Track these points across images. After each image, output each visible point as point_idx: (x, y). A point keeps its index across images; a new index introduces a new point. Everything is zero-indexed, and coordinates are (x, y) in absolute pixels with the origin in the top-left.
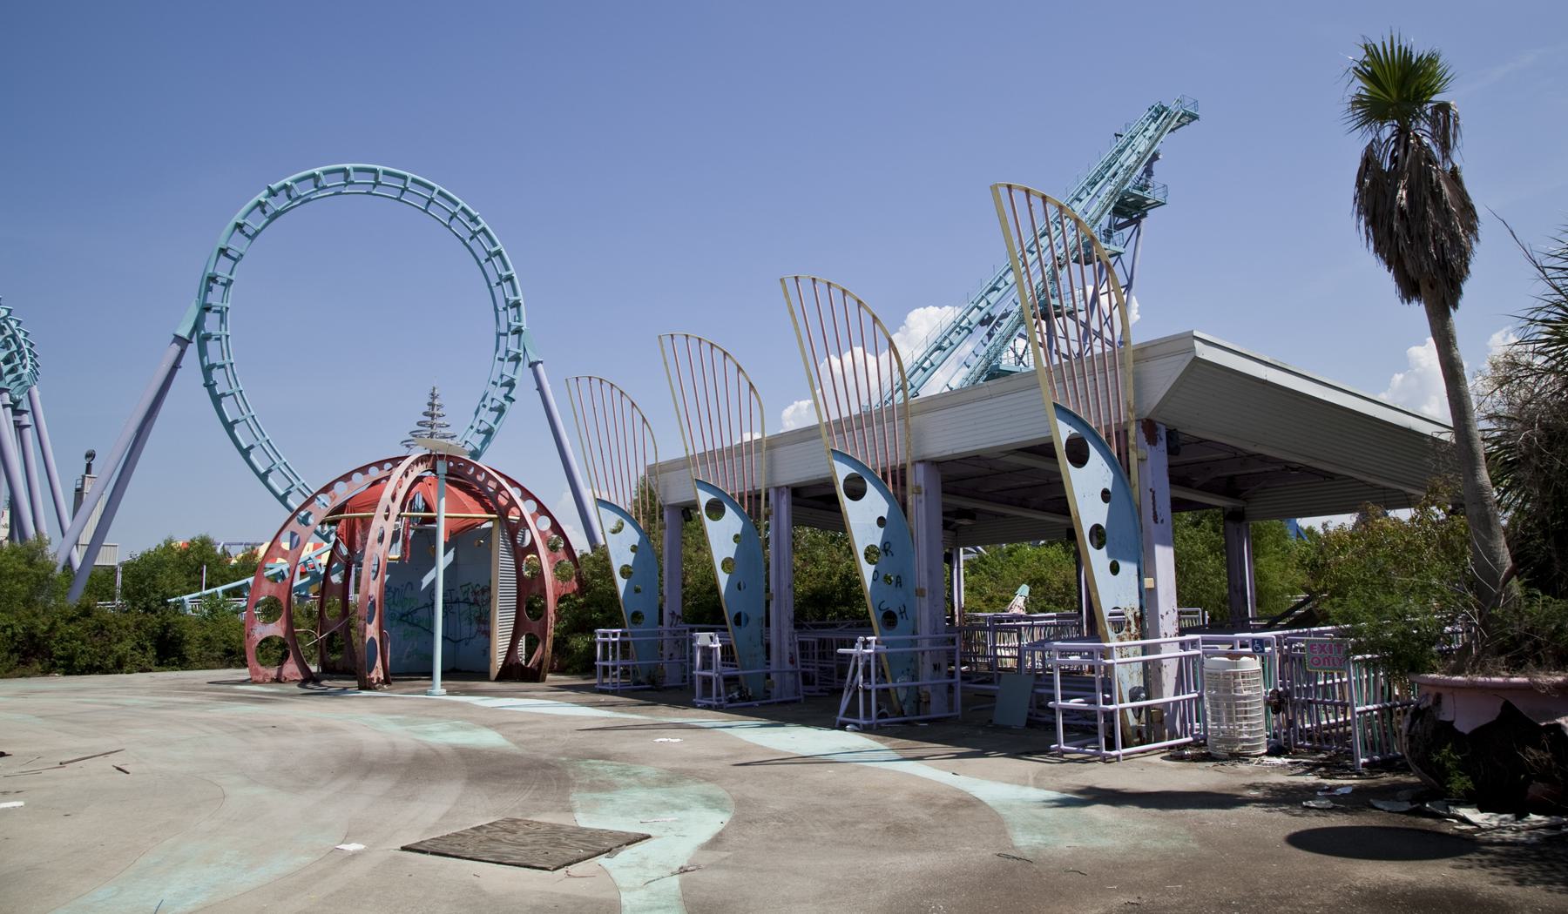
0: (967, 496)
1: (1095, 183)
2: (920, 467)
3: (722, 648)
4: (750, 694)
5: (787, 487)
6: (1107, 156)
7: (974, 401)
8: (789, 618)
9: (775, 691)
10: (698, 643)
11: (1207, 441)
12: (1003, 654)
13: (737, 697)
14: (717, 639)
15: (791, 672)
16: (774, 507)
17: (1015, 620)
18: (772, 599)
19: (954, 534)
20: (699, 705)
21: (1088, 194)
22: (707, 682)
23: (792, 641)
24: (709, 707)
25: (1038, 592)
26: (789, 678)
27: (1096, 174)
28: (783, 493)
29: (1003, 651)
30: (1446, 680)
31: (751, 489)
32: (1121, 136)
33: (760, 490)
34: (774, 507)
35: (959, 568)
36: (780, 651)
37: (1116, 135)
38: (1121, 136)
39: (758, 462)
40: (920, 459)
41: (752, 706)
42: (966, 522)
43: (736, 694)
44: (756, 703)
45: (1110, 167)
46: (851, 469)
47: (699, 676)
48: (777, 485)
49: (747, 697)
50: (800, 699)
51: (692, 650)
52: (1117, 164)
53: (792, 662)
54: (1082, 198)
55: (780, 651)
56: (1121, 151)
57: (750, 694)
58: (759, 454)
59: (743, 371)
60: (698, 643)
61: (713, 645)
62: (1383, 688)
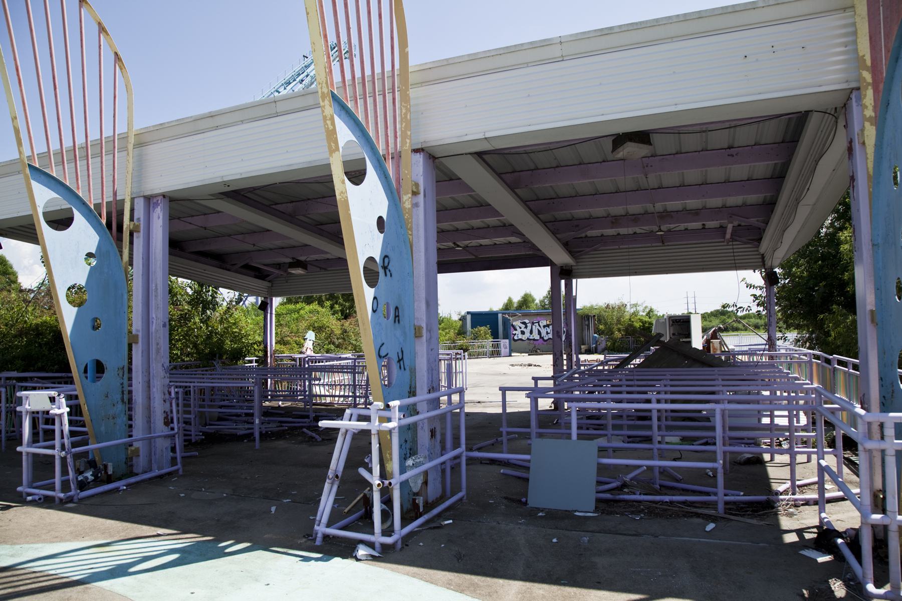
0: (531, 210)
1: (290, 83)
2: (419, 158)
3: (70, 414)
4: (110, 472)
5: (164, 196)
6: (297, 68)
7: (527, 65)
8: (163, 366)
9: (141, 462)
10: (27, 407)
11: (213, 266)
12: (323, 393)
13: (91, 478)
14: (63, 400)
15: (166, 437)
16: (142, 222)
17: (324, 361)
18: (137, 343)
19: (269, 284)
20: (29, 498)
21: (285, 89)
22: (43, 465)
23: (167, 396)
24: (47, 503)
25: (39, 309)
26: (163, 445)
27: (291, 78)
28: (157, 204)
29: (322, 388)
30: (236, 349)
31: (111, 199)
32: (307, 58)
33: (123, 201)
34: (142, 222)
35: (271, 314)
36: (148, 409)
37: (304, 56)
38: (307, 58)
39: (125, 163)
40: (419, 146)
41: (117, 490)
42: (299, 271)
43: (89, 475)
44: (121, 484)
45: (299, 75)
46: (353, 136)
47: (28, 453)
48: (148, 193)
49: (105, 478)
50: (178, 470)
51: (19, 416)
52: (305, 74)
53: (168, 421)
54: (280, 91)
55: (148, 409)
56: (307, 67)
57: (110, 472)
58: (125, 153)
59: (106, 32)
60: (27, 407)
61: (55, 411)
62: (684, 440)
